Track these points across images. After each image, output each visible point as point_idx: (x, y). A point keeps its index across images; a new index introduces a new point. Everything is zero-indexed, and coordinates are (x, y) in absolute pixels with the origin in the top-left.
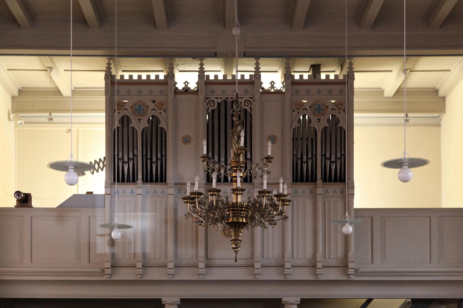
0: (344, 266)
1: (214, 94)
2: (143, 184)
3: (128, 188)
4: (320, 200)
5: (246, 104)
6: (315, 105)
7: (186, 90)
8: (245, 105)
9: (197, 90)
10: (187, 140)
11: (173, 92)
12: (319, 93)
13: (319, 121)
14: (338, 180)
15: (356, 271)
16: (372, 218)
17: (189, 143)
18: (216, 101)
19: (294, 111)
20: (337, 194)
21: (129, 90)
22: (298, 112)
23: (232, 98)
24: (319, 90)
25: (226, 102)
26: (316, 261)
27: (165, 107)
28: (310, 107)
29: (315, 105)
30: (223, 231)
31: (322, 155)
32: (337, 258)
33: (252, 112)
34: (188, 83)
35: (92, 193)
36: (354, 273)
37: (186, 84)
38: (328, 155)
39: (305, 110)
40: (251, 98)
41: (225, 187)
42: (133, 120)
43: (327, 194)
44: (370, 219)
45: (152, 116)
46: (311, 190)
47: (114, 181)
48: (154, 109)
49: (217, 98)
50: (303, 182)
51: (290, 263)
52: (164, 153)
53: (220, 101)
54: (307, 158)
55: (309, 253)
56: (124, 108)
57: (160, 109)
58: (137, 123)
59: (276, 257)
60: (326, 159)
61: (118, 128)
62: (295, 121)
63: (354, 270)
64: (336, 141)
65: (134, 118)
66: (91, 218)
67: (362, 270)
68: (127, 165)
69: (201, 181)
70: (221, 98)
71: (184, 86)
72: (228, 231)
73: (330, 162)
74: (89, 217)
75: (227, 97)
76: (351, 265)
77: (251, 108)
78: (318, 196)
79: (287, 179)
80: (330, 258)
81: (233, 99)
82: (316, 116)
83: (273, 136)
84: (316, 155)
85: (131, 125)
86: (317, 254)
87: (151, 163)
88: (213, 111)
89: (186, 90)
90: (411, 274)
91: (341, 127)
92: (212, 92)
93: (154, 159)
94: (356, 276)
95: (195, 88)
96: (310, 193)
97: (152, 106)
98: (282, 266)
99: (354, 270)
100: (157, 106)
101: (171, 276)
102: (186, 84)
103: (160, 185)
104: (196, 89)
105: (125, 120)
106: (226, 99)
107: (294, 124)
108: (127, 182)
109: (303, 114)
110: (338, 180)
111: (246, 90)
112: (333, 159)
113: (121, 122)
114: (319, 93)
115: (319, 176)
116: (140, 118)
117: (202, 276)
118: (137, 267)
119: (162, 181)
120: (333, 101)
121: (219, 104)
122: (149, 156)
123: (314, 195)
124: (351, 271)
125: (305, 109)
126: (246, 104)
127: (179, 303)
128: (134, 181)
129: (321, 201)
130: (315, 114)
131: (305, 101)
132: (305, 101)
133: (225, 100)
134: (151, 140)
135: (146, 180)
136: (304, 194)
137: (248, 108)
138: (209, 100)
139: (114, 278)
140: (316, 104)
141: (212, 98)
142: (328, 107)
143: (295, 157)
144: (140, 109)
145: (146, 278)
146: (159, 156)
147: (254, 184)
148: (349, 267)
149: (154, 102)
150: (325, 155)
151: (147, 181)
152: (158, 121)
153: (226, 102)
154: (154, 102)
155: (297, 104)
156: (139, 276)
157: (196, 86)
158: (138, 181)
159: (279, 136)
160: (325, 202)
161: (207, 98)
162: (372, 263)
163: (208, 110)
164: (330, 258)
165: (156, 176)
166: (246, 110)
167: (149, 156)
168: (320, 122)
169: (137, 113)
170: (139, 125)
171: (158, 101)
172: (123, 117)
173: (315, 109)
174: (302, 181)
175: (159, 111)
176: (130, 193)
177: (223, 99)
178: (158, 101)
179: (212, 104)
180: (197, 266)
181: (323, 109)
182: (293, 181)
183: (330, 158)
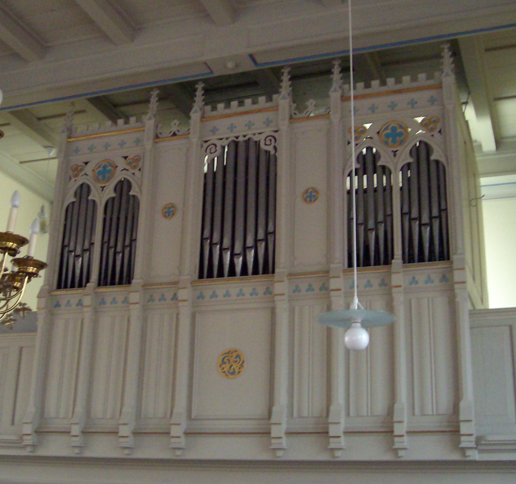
0: (452, 430)
3: (221, 287)
4: (399, 298)
5: (268, 142)
6: (387, 128)
11: (287, 119)
12: (106, 148)
14: (372, 261)
16: (511, 327)
17: (173, 214)
18: (219, 143)
20: (117, 305)
23: (245, 136)
24: (412, 100)
25: (236, 144)
26: (393, 423)
27: (140, 163)
28: (378, 133)
29: (387, 128)
30: (221, 366)
36: (473, 445)
38: (415, 214)
43: (413, 286)
44: (507, 328)
45: (420, 142)
46: (383, 280)
47: (350, 265)
49: (221, 139)
50: (369, 265)
55: (380, 406)
56: (83, 173)
57: (134, 167)
58: (401, 154)
60: (411, 220)
61: (356, 170)
63: (473, 438)
64: (430, 188)
67: (490, 438)
70: (227, 139)
72: (228, 366)
73: (420, 225)
74: (21, 349)
75: (237, 135)
76: (464, 428)
77: (275, 148)
78: (394, 290)
79: (337, 261)
81: (247, 138)
82: (391, 147)
83: (312, 188)
84: (392, 215)
85: (433, 157)
91: (437, 162)
93: (119, 248)
94: (481, 451)
96: (441, 281)
97: (122, 164)
100: (129, 164)
101: (126, 451)
105: (84, 190)
106: (235, 139)
108: (264, 273)
109: (367, 145)
110: (372, 261)
112: (425, 219)
113: (78, 196)
116: (103, 185)
117: (178, 453)
118: (120, 434)
120: (419, 119)
122: (112, 243)
123: (386, 284)
124: (465, 442)
128: (387, 262)
130: (386, 143)
131: (368, 126)
132: (368, 126)
135: (409, 259)
137: (270, 148)
138: (209, 143)
139: (41, 452)
140: (388, 127)
141: (214, 139)
143: (106, 246)
144: (105, 171)
145: (88, 454)
147: (452, 263)
148: (462, 431)
149: (126, 158)
152: (429, 150)
156: (77, 451)
158: (393, 261)
159: (321, 187)
160: (410, 300)
161: (206, 142)
164: (423, 414)
166: (267, 152)
167: (112, 243)
168: (397, 156)
169: (101, 177)
170: (102, 195)
171: (131, 157)
172: (82, 185)
173: (388, 136)
174: (421, 259)
177: (230, 140)
178: (131, 157)
180: (68, 433)
182: (201, 276)
183: (420, 218)
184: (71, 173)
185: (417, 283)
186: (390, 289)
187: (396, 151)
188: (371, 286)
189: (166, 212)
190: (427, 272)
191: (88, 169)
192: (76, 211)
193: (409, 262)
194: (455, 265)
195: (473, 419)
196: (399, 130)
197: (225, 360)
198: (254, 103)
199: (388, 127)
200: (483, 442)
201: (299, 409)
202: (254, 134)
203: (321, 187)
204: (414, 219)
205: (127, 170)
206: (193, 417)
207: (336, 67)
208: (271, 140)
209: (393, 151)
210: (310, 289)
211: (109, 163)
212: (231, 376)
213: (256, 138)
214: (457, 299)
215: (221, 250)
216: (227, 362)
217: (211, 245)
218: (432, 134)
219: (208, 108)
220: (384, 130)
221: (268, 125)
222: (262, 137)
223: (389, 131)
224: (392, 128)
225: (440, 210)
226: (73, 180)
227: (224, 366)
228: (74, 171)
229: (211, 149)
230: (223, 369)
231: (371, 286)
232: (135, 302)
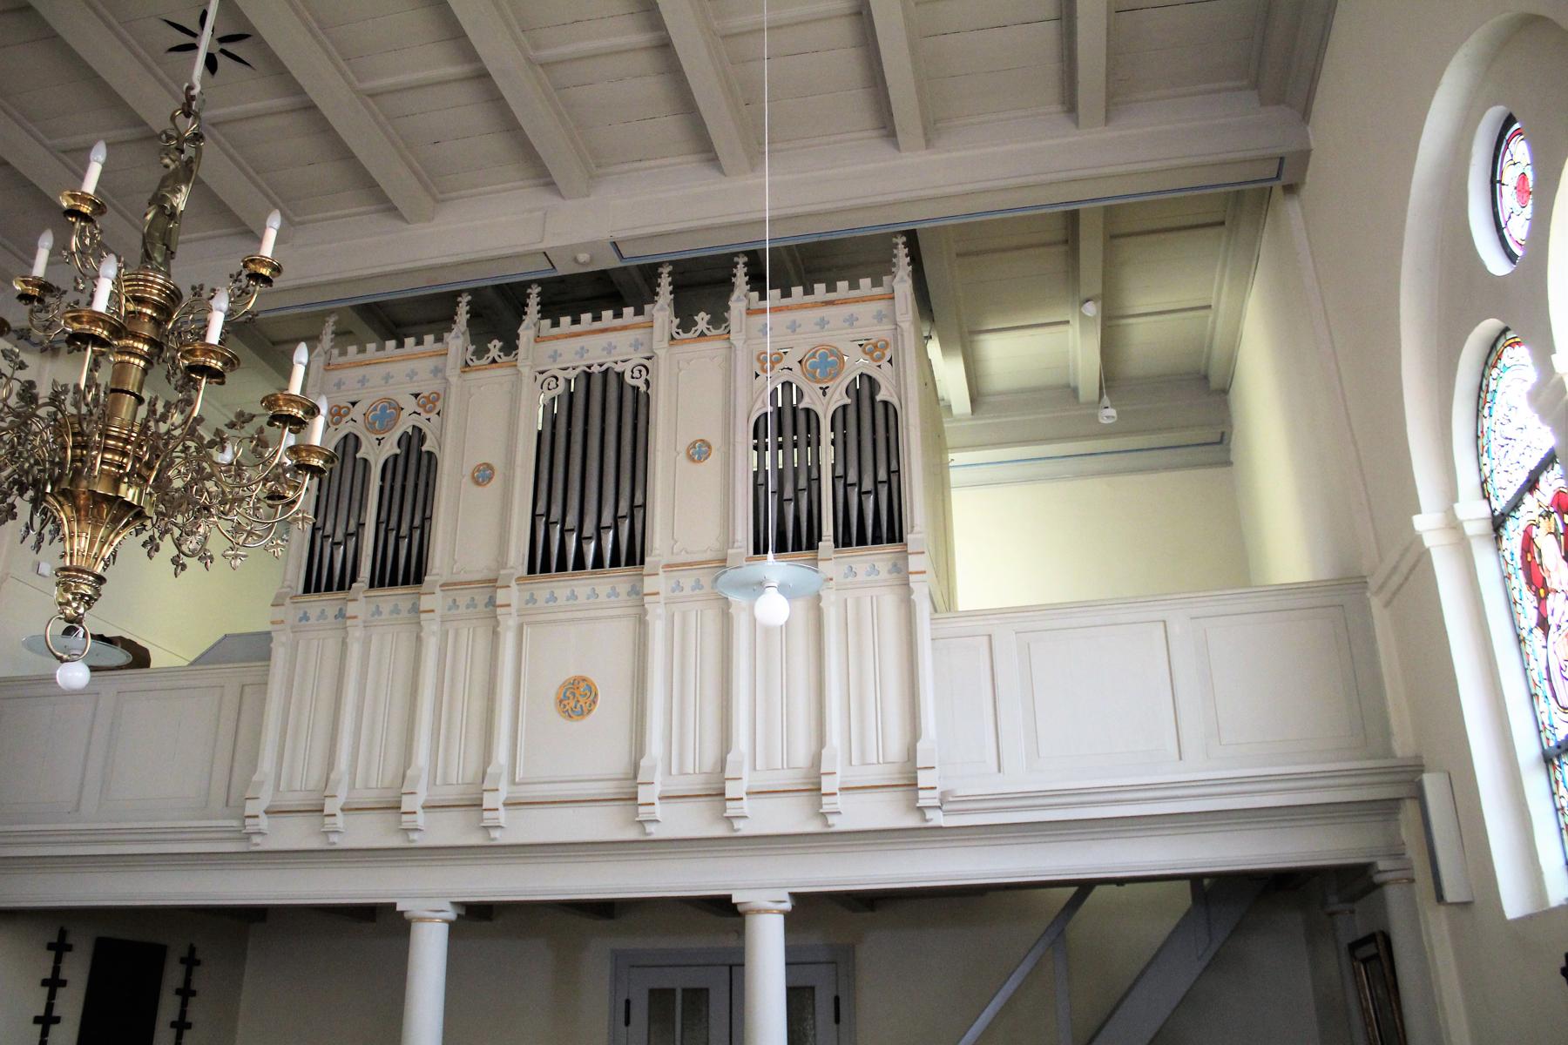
5: (636, 374)
10: (483, 475)
14: (430, 952)
21: (823, 319)
24: (823, 319)
27: (439, 405)
29: (813, 356)
31: (834, 478)
38: (852, 477)
44: (986, 639)
46: (895, 565)
54: (796, 490)
66: (247, 689)
76: (924, 779)
78: (912, 577)
80: (864, 764)
85: (879, 398)
87: (398, 538)
91: (886, 403)
93: (404, 530)
96: (890, 572)
97: (410, 404)
98: (816, 790)
100: (423, 406)
107: (759, 404)
110: (430, 952)
112: (868, 484)
119: (891, 540)
122: (393, 523)
124: (925, 799)
126: (636, 374)
127: (788, 906)
128: (812, 546)
134: (403, 488)
135: (844, 540)
137: (640, 383)
149: (416, 396)
151: (847, 544)
152: (873, 384)
154: (416, 396)
161: (542, 373)
164: (864, 764)
165: (403, 569)
166: (636, 389)
167: (393, 523)
172: (346, 437)
175: (425, 415)
181: (832, 364)
190: (872, 561)
191: (357, 413)
201: (445, 774)
203: (716, 440)
213: (618, 368)
225: (889, 472)
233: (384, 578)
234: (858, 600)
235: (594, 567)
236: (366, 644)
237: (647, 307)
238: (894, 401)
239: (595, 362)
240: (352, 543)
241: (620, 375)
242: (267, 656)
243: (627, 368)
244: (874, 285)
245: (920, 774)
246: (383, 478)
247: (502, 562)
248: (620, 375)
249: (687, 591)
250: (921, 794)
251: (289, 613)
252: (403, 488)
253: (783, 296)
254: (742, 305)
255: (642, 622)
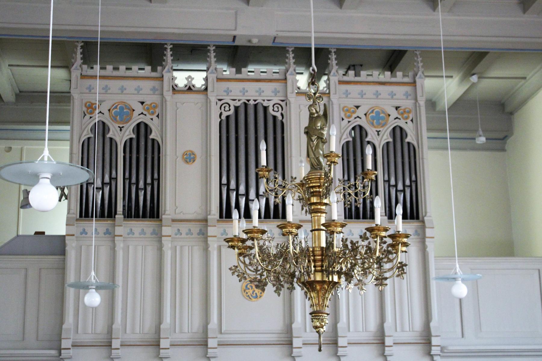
1: (230, 94)
2: (124, 220)
4: (120, 244)
5: (276, 109)
6: (372, 112)
7: (190, 89)
8: (273, 110)
9: (206, 89)
10: (189, 158)
12: (392, 98)
13: (378, 134)
14: (272, 216)
15: (442, 349)
16: (539, 270)
18: (232, 103)
19: (343, 119)
20: (146, 236)
22: (349, 122)
23: (255, 101)
25: (246, 105)
26: (160, 338)
27: (158, 111)
28: (365, 114)
29: (372, 112)
30: (245, 291)
31: (384, 181)
32: (413, 331)
33: (284, 121)
34: (193, 79)
35: (43, 233)
36: (439, 352)
37: (190, 80)
38: (393, 182)
39: (358, 119)
40: (282, 101)
41: (224, 226)
42: (111, 128)
44: (537, 271)
46: (200, 230)
48: (142, 113)
51: (216, 340)
52: (156, 176)
53: (238, 104)
54: (145, 184)
55: (373, 325)
59: (195, 330)
60: (389, 186)
62: (86, 129)
63: (439, 348)
64: (146, 159)
65: (113, 126)
67: (451, 348)
68: (402, 194)
69: (70, 216)
71: (186, 82)
72: (251, 291)
76: (434, 341)
78: (209, 239)
82: (375, 127)
85: (109, 136)
86: (339, 325)
87: (137, 189)
88: (228, 117)
89: (190, 89)
90: (521, 354)
92: (228, 91)
93: (141, 184)
95: (202, 85)
97: (139, 108)
99: (439, 348)
100: (148, 109)
102: (190, 80)
103: (355, 222)
104: (204, 87)
106: (247, 102)
107: (85, 133)
110: (272, 216)
111: (276, 89)
114: (392, 98)
115: (120, 208)
116: (121, 126)
121: (237, 109)
122: (134, 180)
123: (111, 235)
125: (358, 117)
126: (276, 109)
129: (170, 245)
133: (245, 103)
136: (142, 236)
137: (278, 115)
141: (227, 99)
142: (389, 115)
146: (149, 181)
147: (161, 220)
149: (142, 103)
150: (389, 181)
153: (246, 105)
154: (142, 103)
155: (348, 111)
157: (204, 82)
161: (220, 100)
162: (463, 337)
163: (221, 115)
164: (403, 331)
165: (149, 210)
166: (275, 117)
167: (134, 180)
168: (381, 135)
170: (121, 135)
171: (148, 102)
173: (373, 119)
175: (149, 117)
176: (187, 234)
177: (241, 102)
178: (148, 102)
179: (227, 109)
181: (383, 118)
182: (81, 216)
183: (396, 186)
184: (84, 109)
185: (181, 234)
186: (207, 238)
187: (123, 127)
188: (145, 234)
189: (186, 158)
191: (360, 112)
192: (91, 147)
193: (128, 217)
194: (427, 224)
195: (71, 337)
196: (382, 115)
197: (248, 286)
198: (116, 69)
199: (117, 106)
200: (445, 351)
202: (264, 100)
203: (196, 147)
204: (106, 184)
205: (145, 115)
206: (223, 331)
207: (79, 48)
208: (278, 108)
209: (377, 131)
210: (190, 232)
211: (126, 106)
212: (253, 299)
213: (265, 104)
214: (209, 249)
215: (237, 195)
216: (250, 288)
217: (228, 190)
218: (406, 121)
219: (85, 67)
220: (114, 109)
221: (276, 95)
222: (271, 104)
223: (374, 114)
224: (377, 112)
225: (111, 178)
226: (88, 116)
227: (247, 291)
228: (88, 108)
229: (225, 107)
230: (247, 293)
231: (145, 234)
232: (167, 234)
233: (131, 213)
234: (181, 247)
235: (265, 218)
236: (126, 250)
237: (159, 68)
238: (415, 144)
239: (252, 98)
240: (107, 190)
241: (265, 109)
242: (63, 252)
243: (271, 104)
244: (404, 76)
245: (162, 341)
246: (124, 152)
247: (208, 212)
248: (265, 109)
249: (184, 235)
250: (161, 351)
251: (74, 230)
252: (355, 161)
253: (356, 76)
254: (78, 73)
255: (160, 249)
